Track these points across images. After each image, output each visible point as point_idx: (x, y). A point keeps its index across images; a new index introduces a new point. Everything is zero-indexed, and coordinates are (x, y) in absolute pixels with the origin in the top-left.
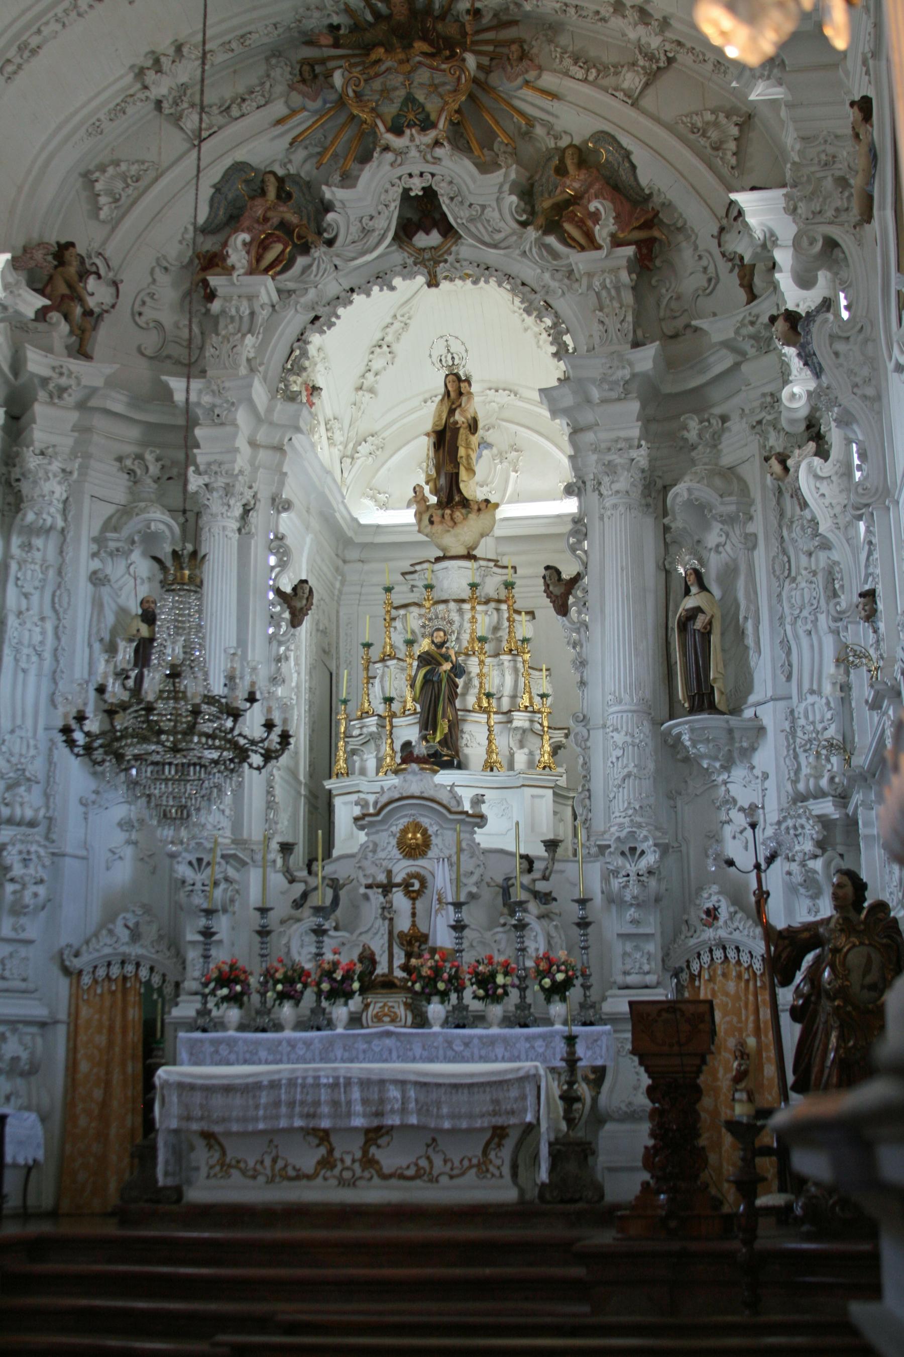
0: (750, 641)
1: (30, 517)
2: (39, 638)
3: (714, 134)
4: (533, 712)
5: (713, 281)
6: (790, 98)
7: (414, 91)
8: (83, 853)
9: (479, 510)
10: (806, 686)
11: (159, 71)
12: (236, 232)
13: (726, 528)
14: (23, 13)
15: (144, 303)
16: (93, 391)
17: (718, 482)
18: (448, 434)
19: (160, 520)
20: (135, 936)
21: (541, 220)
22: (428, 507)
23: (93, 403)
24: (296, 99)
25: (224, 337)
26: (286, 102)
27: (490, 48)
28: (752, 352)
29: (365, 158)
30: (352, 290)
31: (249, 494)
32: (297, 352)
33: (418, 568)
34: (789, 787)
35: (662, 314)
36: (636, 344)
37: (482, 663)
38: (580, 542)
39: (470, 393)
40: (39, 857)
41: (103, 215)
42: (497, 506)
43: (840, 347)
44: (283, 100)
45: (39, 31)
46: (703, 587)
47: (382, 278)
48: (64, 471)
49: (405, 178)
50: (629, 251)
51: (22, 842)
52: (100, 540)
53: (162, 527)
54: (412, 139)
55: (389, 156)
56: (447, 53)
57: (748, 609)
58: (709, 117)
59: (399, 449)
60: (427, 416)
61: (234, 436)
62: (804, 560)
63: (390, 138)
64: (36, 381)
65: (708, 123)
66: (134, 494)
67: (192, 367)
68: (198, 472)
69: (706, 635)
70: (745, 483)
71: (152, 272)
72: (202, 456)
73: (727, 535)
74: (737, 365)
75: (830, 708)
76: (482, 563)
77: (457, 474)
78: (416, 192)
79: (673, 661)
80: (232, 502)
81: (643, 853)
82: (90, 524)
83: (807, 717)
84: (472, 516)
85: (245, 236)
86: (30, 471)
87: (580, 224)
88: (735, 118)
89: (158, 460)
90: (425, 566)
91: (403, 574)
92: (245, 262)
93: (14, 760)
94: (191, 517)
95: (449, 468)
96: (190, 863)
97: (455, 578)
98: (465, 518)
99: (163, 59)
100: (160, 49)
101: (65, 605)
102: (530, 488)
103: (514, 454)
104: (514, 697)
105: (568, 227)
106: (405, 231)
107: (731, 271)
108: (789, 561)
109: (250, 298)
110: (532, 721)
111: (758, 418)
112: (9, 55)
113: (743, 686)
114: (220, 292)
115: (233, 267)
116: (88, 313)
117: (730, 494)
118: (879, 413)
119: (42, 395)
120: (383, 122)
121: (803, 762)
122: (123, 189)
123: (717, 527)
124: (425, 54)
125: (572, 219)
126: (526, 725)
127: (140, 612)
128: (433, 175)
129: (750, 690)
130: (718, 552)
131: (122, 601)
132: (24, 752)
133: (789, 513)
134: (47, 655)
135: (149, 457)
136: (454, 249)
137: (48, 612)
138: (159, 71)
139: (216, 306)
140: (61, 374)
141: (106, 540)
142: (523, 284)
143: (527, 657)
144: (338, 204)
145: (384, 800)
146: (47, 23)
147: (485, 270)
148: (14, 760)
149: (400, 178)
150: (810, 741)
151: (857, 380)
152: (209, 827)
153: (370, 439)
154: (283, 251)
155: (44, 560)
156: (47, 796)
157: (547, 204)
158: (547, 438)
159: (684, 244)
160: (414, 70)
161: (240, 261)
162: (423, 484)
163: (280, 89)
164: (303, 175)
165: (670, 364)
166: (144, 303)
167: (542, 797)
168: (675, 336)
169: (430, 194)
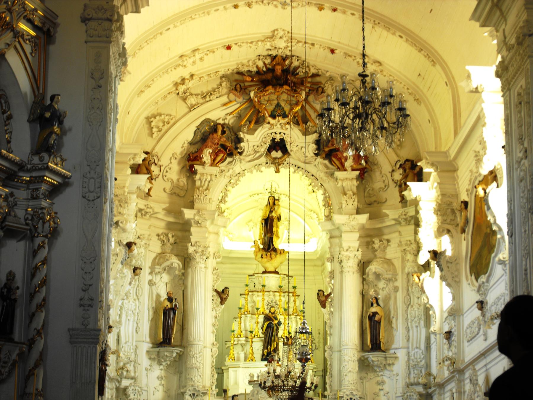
0: (394, 325)
2: (135, 307)
5: (387, 186)
7: (280, 102)
9: (280, 253)
10: (415, 346)
12: (206, 148)
13: (386, 282)
15: (167, 172)
18: (269, 221)
19: (176, 262)
24: (232, 97)
25: (201, 191)
26: (228, 97)
34: (407, 380)
35: (366, 194)
38: (331, 280)
39: (279, 205)
40: (138, 391)
41: (154, 136)
43: (449, 265)
44: (226, 96)
46: (378, 304)
49: (273, 134)
50: (357, 173)
54: (279, 121)
55: (268, 126)
57: (394, 314)
62: (416, 299)
63: (270, 119)
69: (379, 322)
70: (395, 266)
72: (193, 239)
73: (387, 285)
75: (423, 354)
76: (282, 276)
77: (272, 238)
78: (278, 140)
79: (364, 328)
83: (414, 356)
84: (278, 256)
87: (339, 159)
89: (173, 236)
90: (259, 275)
92: (209, 161)
93: (126, 354)
94: (187, 260)
96: (190, 395)
97: (272, 281)
98: (276, 256)
101: (141, 294)
107: (396, 187)
108: (410, 299)
111: (404, 248)
113: (390, 340)
114: (198, 171)
115: (205, 162)
117: (390, 271)
118: (459, 286)
120: (268, 113)
121: (412, 372)
122: (163, 126)
125: (336, 157)
128: (284, 134)
129: (393, 342)
130: (383, 290)
131: (159, 291)
132: (129, 351)
134: (136, 314)
137: (135, 297)
140: (148, 208)
142: (313, 175)
144: (245, 140)
148: (126, 354)
149: (272, 133)
150: (415, 365)
151: (454, 276)
152: (196, 382)
157: (327, 149)
159: (377, 170)
161: (207, 160)
162: (258, 240)
163: (225, 91)
168: (370, 204)
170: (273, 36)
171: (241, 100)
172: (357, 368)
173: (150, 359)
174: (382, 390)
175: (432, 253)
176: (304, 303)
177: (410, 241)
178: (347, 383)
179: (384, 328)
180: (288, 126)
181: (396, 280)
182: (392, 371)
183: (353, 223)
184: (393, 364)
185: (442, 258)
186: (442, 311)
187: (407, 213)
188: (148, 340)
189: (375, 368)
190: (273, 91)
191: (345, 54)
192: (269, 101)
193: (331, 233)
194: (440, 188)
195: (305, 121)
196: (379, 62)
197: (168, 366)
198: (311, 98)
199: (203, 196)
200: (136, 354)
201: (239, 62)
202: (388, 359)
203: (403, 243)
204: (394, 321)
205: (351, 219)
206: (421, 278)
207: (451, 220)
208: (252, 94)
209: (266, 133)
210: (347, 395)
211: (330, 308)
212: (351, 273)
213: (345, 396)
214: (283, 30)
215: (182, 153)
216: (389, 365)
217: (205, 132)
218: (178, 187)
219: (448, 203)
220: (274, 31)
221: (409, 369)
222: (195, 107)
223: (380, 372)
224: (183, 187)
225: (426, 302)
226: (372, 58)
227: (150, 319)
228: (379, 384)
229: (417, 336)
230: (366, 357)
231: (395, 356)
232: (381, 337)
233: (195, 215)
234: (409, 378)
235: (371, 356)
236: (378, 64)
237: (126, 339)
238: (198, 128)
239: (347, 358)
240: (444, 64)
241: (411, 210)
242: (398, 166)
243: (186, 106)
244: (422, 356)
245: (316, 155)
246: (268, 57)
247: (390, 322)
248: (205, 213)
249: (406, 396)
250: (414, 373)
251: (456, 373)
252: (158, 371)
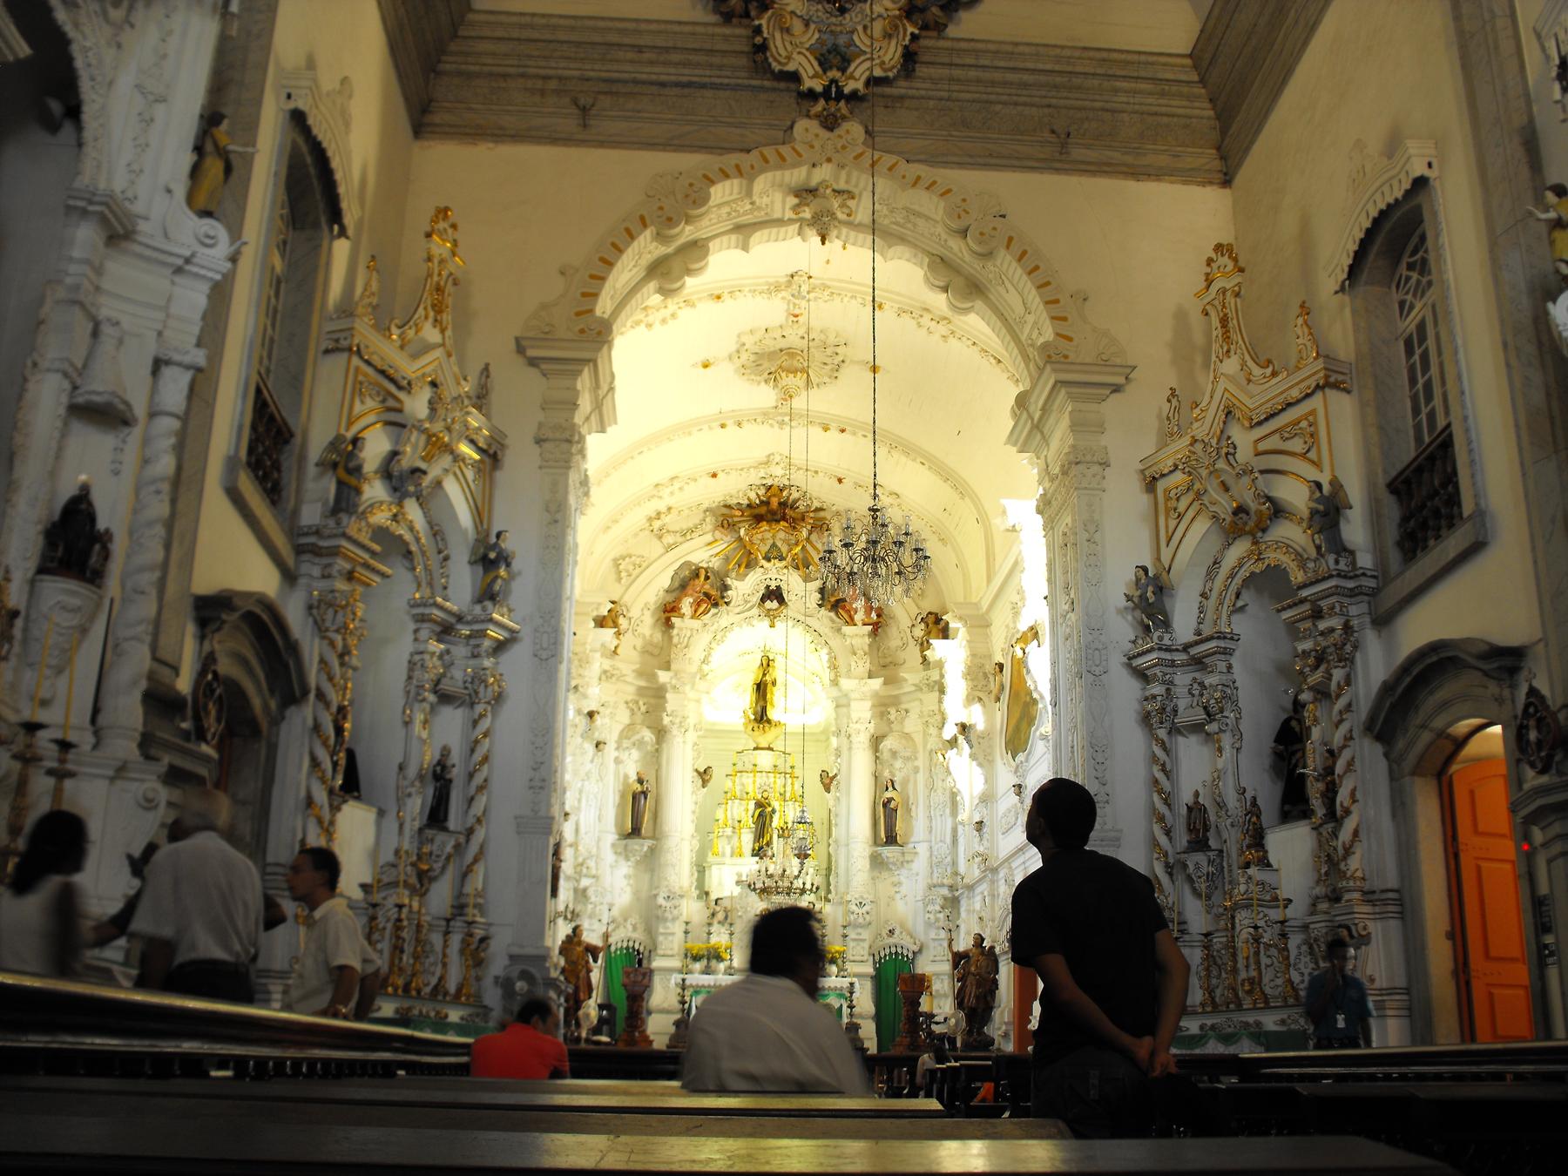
19: (648, 736)
20: (635, 928)
63: (763, 562)
72: (669, 707)
94: (661, 733)
183: (865, 689)
188: (613, 829)
197: (638, 862)
208: (742, 532)
218: (651, 644)
239: (856, 854)
247: (909, 810)
252: (625, 868)
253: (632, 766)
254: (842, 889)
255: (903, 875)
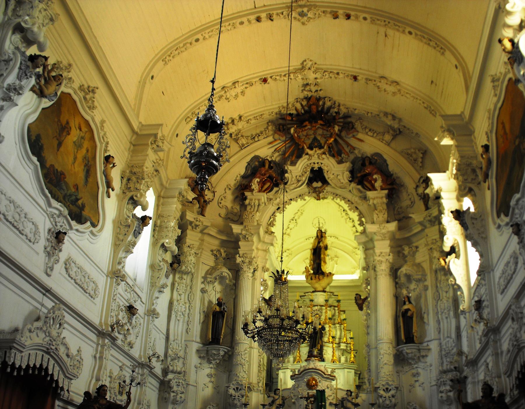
0: (426, 320)
1: (184, 268)
2: (184, 309)
3: (414, 156)
4: (347, 344)
5: (413, 203)
6: (456, 144)
8: (195, 384)
10: (446, 335)
11: (233, 124)
14: (195, 102)
15: (222, 199)
16: (207, 227)
17: (415, 268)
18: (318, 251)
19: (226, 272)
21: (357, 181)
22: (310, 274)
23: (204, 232)
24: (277, 136)
26: (273, 137)
27: (342, 124)
28: (428, 225)
29: (299, 157)
30: (291, 200)
31: (256, 265)
32: (272, 219)
33: (306, 294)
34: (441, 368)
35: (395, 212)
36: (388, 222)
37: (330, 326)
38: (367, 286)
40: (182, 384)
42: (333, 274)
45: (199, 108)
46: (410, 302)
47: (301, 196)
48: (195, 253)
50: (386, 192)
51: (177, 379)
52: (205, 278)
53: (226, 274)
54: (316, 151)
55: (307, 156)
56: (328, 125)
58: (413, 150)
59: (297, 255)
60: (310, 244)
61: (253, 245)
62: (444, 294)
64: (188, 222)
65: (412, 152)
66: (217, 263)
67: (240, 221)
68: (239, 256)
69: (411, 318)
71: (225, 189)
72: (241, 251)
73: (418, 286)
74: (422, 230)
79: (399, 326)
80: (251, 267)
81: (390, 390)
82: (202, 273)
84: (325, 278)
85: (258, 180)
86: (184, 252)
87: (370, 182)
88: (421, 151)
89: (225, 252)
90: (309, 293)
91: (301, 296)
92: (257, 188)
93: (174, 351)
94: (237, 272)
95: (317, 261)
96: (234, 389)
97: (320, 298)
98: (323, 278)
99: (235, 120)
100: (234, 117)
102: (345, 269)
103: (336, 258)
104: (340, 339)
105: (366, 183)
106: (310, 181)
109: (259, 200)
110: (347, 347)
111: (431, 247)
112: (189, 115)
113: (423, 334)
114: (248, 197)
115: (253, 189)
116: (205, 201)
117: (419, 272)
119: (190, 227)
121: (445, 360)
123: (414, 283)
124: (321, 125)
125: (367, 181)
126: (345, 348)
127: (217, 302)
131: (211, 298)
133: (439, 279)
134: (186, 315)
135: (222, 251)
136: (326, 188)
137: (187, 301)
138: (233, 124)
139: (247, 202)
140: (197, 221)
141: (207, 278)
142: (349, 201)
143: (345, 325)
144: (289, 171)
145: (302, 369)
146: (202, 106)
147: (336, 195)
152: (240, 377)
153: (287, 251)
154: (270, 186)
155: (186, 283)
156: (184, 364)
157: (359, 175)
158: (348, 254)
160: (317, 129)
163: (271, 133)
164: (277, 161)
165: (400, 228)
166: (222, 199)
167: (350, 372)
169: (320, 170)
170: (303, 67)
171: (284, 139)
172: (392, 361)
173: (200, 357)
174: (417, 381)
175: (455, 213)
176: (213, 82)
177: (435, 240)
178: (383, 374)
179: (417, 324)
180: (324, 156)
181: (426, 280)
182: (426, 362)
183: (384, 231)
184: (427, 356)
185: (466, 216)
186: (470, 288)
187: (431, 214)
188: (198, 340)
189: (410, 361)
190: (309, 127)
191: (367, 79)
192: (307, 136)
193: (365, 246)
194: (458, 151)
195: (339, 153)
196: (396, 82)
197: (218, 365)
198: (343, 134)
199: (251, 215)
200: (185, 352)
201: (280, 105)
202: (421, 351)
203: (429, 243)
204: (425, 316)
205: (382, 228)
206: (447, 260)
207: (472, 179)
208: (292, 131)
209: (306, 164)
210: (383, 385)
211: (367, 310)
212: (383, 275)
213: (381, 386)
214: (311, 61)
215: (235, 184)
216: (423, 357)
217: (254, 168)
218: (232, 213)
219: (468, 163)
220: (303, 63)
221: (442, 358)
222: (246, 146)
223: (415, 364)
224: (236, 213)
225: (453, 283)
226: (390, 80)
227: (202, 321)
228: (414, 376)
229: (448, 327)
230: (400, 350)
231: (428, 347)
232: (414, 331)
233: (242, 230)
234: (442, 366)
235: (405, 348)
236: (395, 84)
237: (174, 336)
238: (249, 164)
239: (382, 352)
240: (455, 51)
241: (434, 211)
242: (421, 181)
243: (238, 145)
244: (454, 345)
245: (350, 181)
246: (304, 100)
247: (422, 318)
248: (251, 228)
249: (439, 382)
250: (447, 361)
251: (490, 333)
252: (207, 370)
253: (215, 292)
254: (373, 377)
255: (420, 368)
